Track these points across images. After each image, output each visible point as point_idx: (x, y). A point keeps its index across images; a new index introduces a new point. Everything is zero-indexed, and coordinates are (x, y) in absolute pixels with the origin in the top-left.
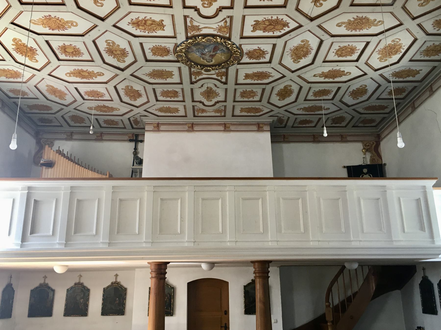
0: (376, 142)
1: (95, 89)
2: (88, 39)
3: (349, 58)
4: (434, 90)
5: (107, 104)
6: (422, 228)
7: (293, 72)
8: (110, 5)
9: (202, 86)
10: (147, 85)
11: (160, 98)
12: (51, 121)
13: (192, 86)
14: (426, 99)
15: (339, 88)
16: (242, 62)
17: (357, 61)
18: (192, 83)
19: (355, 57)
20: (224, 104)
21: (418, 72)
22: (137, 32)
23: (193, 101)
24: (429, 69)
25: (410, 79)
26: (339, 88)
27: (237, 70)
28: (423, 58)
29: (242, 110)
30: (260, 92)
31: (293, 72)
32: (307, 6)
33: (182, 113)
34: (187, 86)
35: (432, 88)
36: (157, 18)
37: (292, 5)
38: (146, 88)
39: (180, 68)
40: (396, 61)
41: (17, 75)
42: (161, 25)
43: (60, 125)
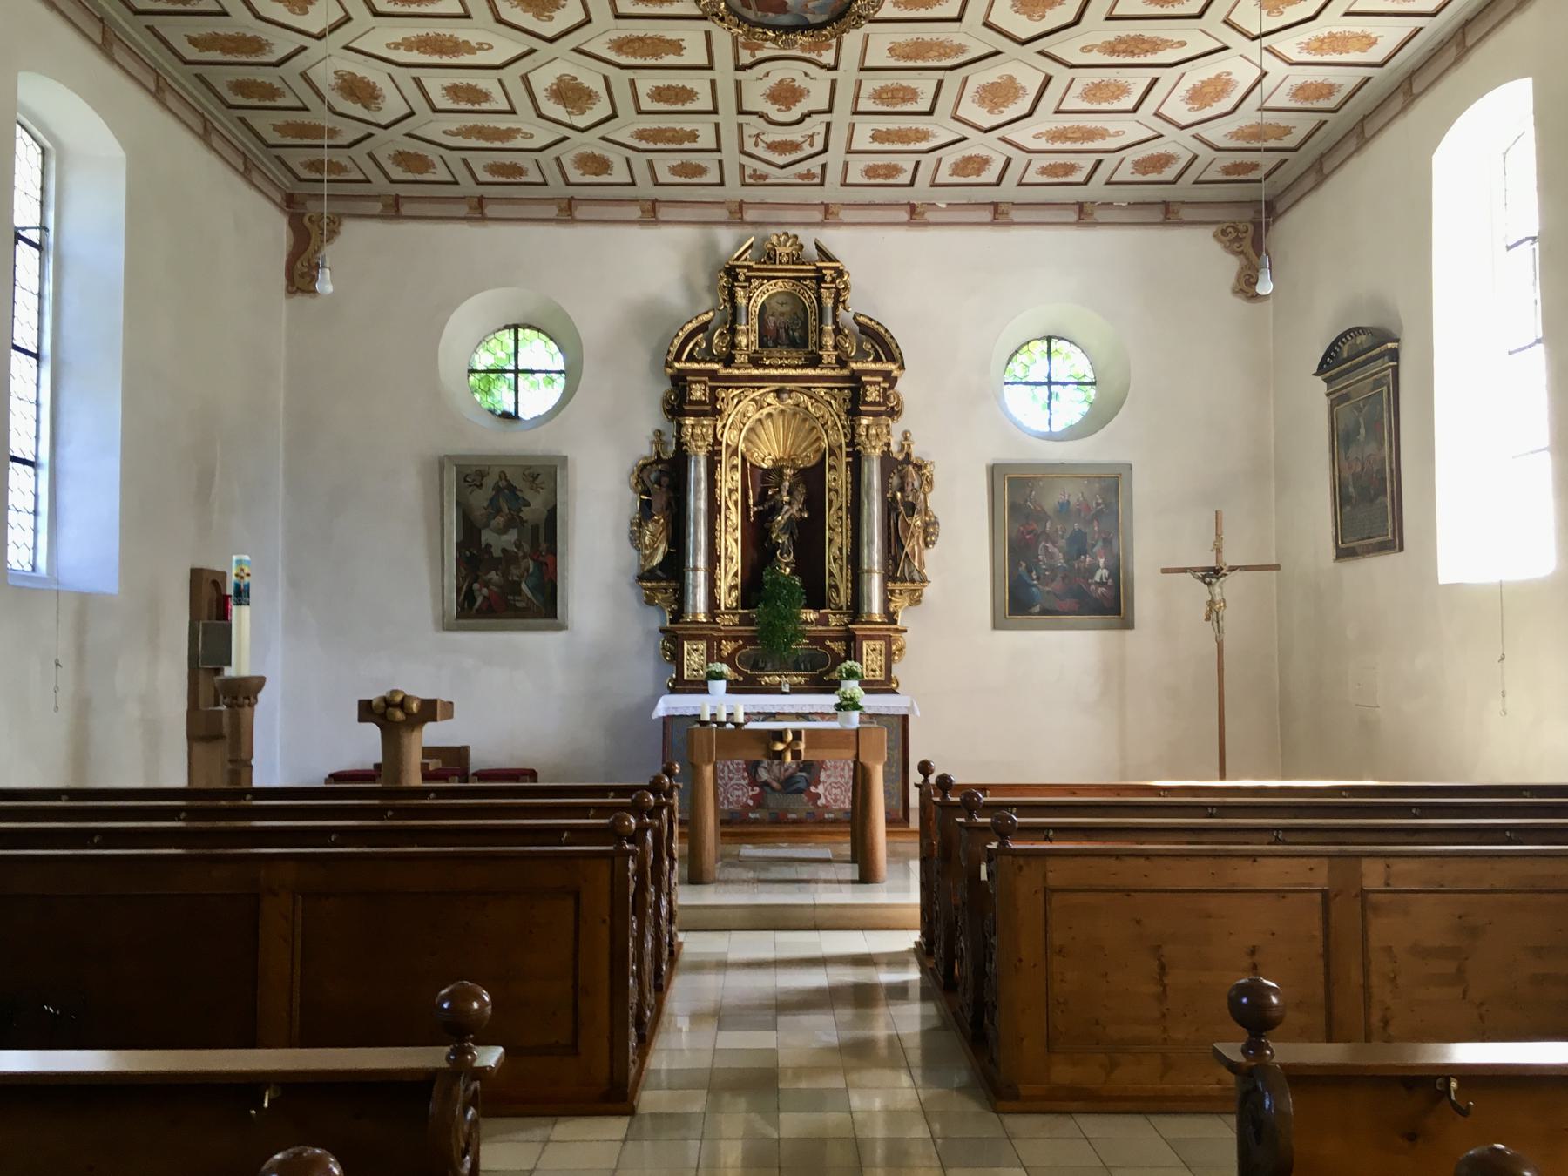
0: (1253, 223)
1: (473, 82)
2: (511, 76)
3: (1116, 106)
4: (1368, 134)
5: (503, 123)
6: (335, 777)
7: (1024, 43)
8: (570, 14)
9: (767, 75)
10: (612, 72)
11: (646, 104)
12: (273, 92)
13: (741, 75)
14: (1349, 157)
15: (1099, 163)
16: (877, 16)
17: (1134, 110)
18: (739, 68)
19: (1129, 103)
20: (826, 118)
21: (1287, 131)
22: (623, 60)
23: (741, 112)
24: (1357, 81)
25: (1272, 143)
26: (1099, 163)
27: (867, 37)
28: (1298, 105)
29: (877, 136)
30: (910, 167)
31: (1024, 43)
32: (1005, 16)
33: (713, 177)
34: (724, 73)
35: (1321, 168)
36: (688, 128)
37: (975, 14)
38: (612, 80)
39: (708, 35)
40: (1229, 108)
41: (257, 45)
42: (693, 136)
43: (299, 104)
